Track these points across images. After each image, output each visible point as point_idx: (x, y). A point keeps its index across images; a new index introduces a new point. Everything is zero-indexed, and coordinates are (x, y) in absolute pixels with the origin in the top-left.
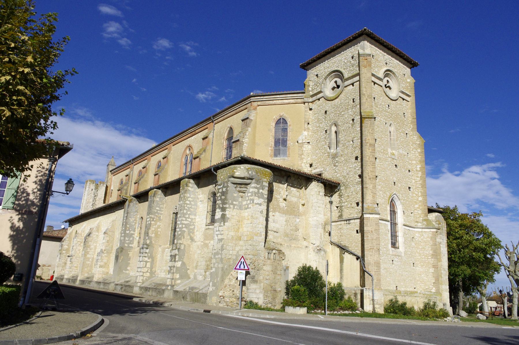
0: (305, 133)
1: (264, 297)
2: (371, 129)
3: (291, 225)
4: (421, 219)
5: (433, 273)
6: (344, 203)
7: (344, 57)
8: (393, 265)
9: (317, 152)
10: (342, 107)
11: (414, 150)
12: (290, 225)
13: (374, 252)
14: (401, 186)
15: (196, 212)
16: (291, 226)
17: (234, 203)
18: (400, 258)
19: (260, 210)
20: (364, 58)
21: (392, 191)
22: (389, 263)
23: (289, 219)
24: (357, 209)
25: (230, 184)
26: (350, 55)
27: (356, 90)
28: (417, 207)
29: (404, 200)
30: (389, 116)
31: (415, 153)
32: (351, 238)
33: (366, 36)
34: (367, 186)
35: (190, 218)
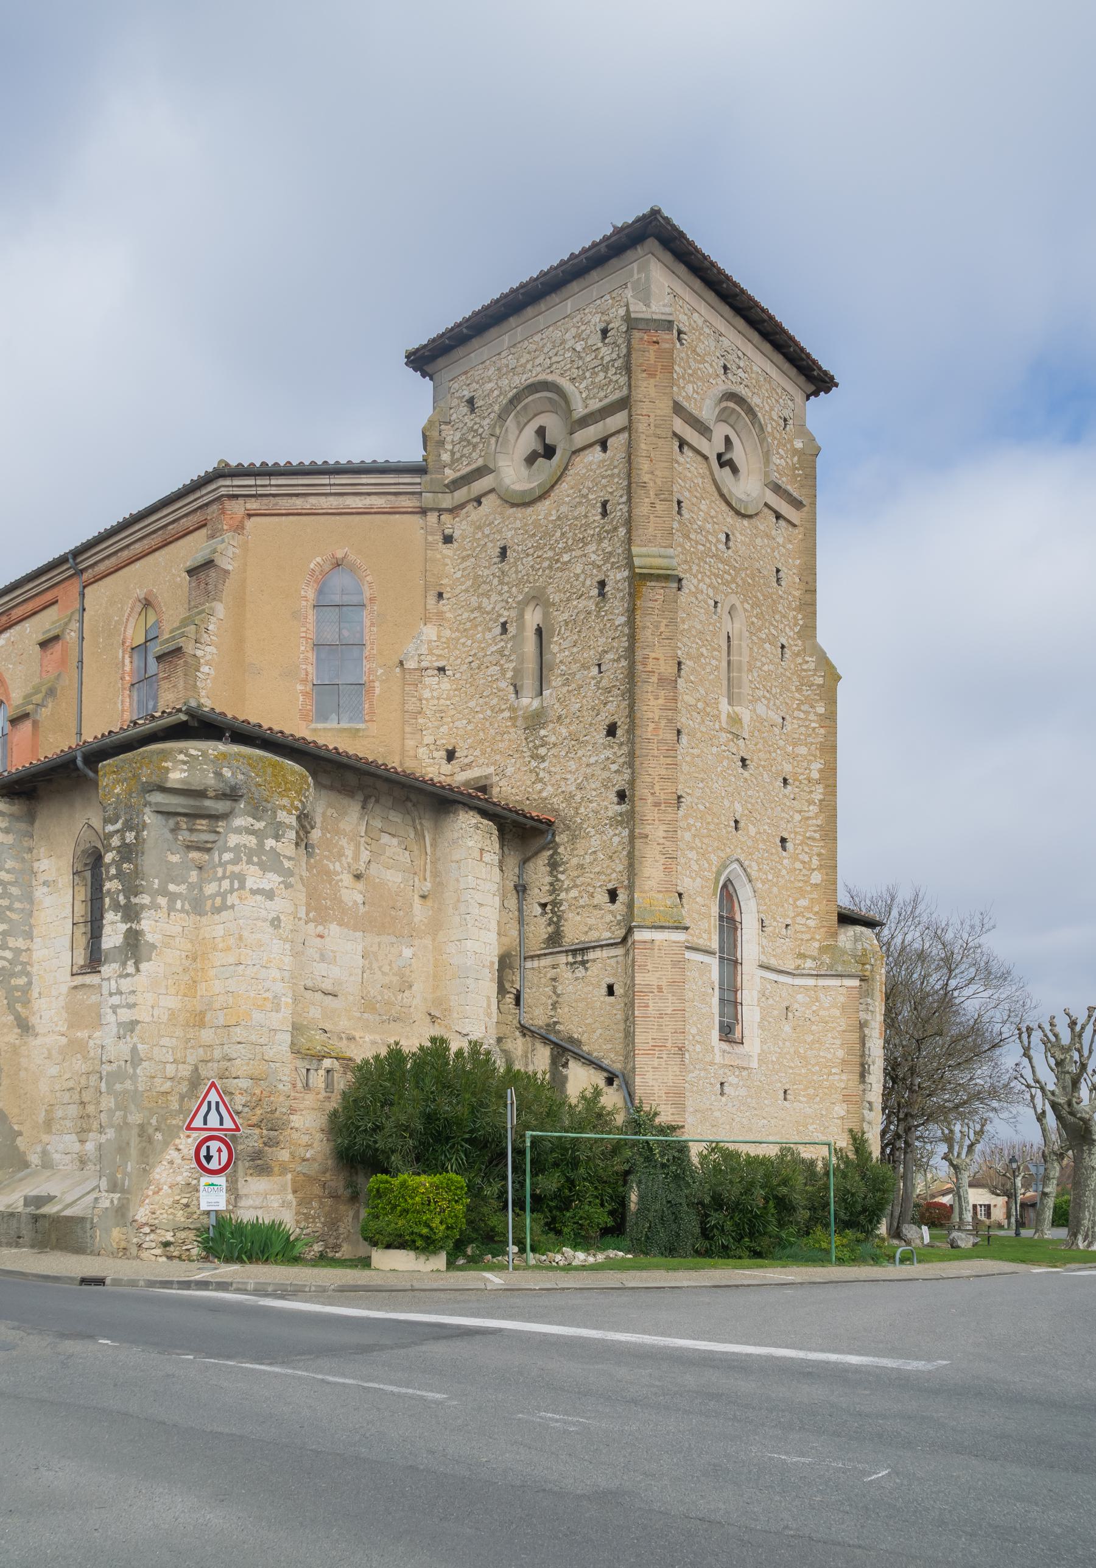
0: (430, 632)
1: (297, 1222)
2: (665, 622)
3: (386, 969)
4: (816, 945)
5: (842, 1118)
6: (567, 890)
7: (574, 331)
8: (724, 1099)
9: (472, 704)
10: (563, 534)
11: (802, 708)
12: (380, 968)
13: (665, 1056)
14: (757, 833)
15: (31, 926)
16: (384, 974)
17: (172, 887)
18: (745, 1073)
19: (270, 918)
20: (646, 337)
21: (728, 850)
22: (711, 1091)
23: (375, 948)
24: (611, 912)
25: (149, 818)
26: (597, 321)
27: (615, 467)
28: (805, 908)
29: (764, 883)
30: (728, 577)
31: (806, 719)
32: (590, 1012)
33: (656, 243)
34: (648, 829)
35: (10, 949)
